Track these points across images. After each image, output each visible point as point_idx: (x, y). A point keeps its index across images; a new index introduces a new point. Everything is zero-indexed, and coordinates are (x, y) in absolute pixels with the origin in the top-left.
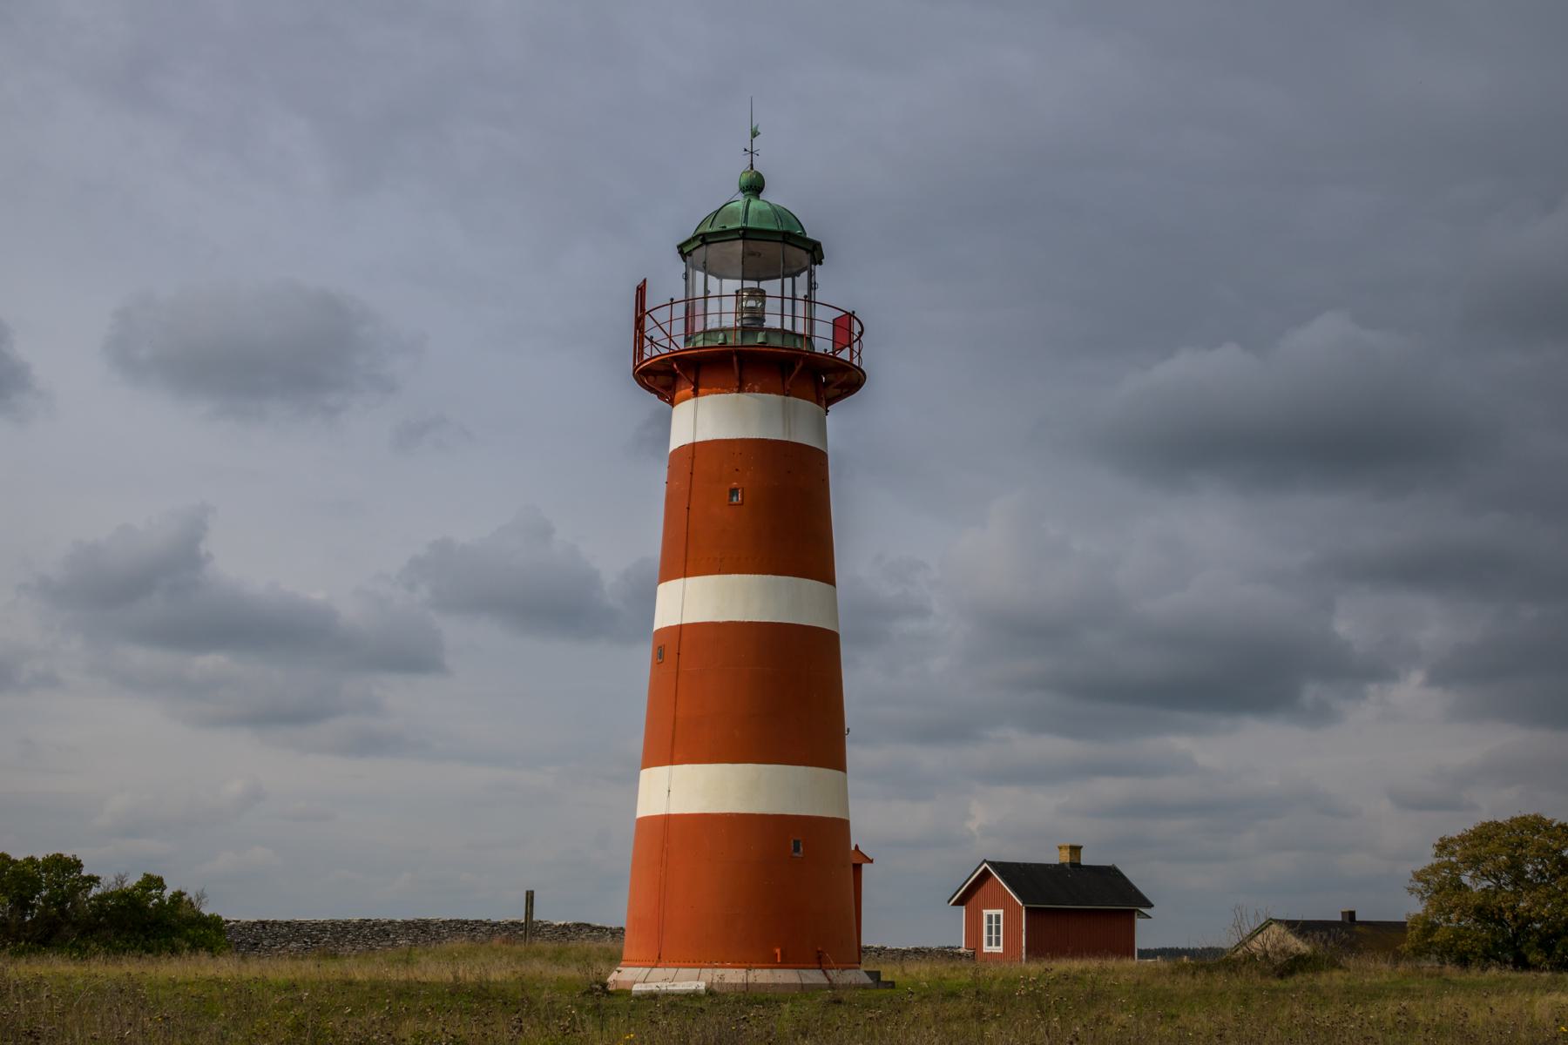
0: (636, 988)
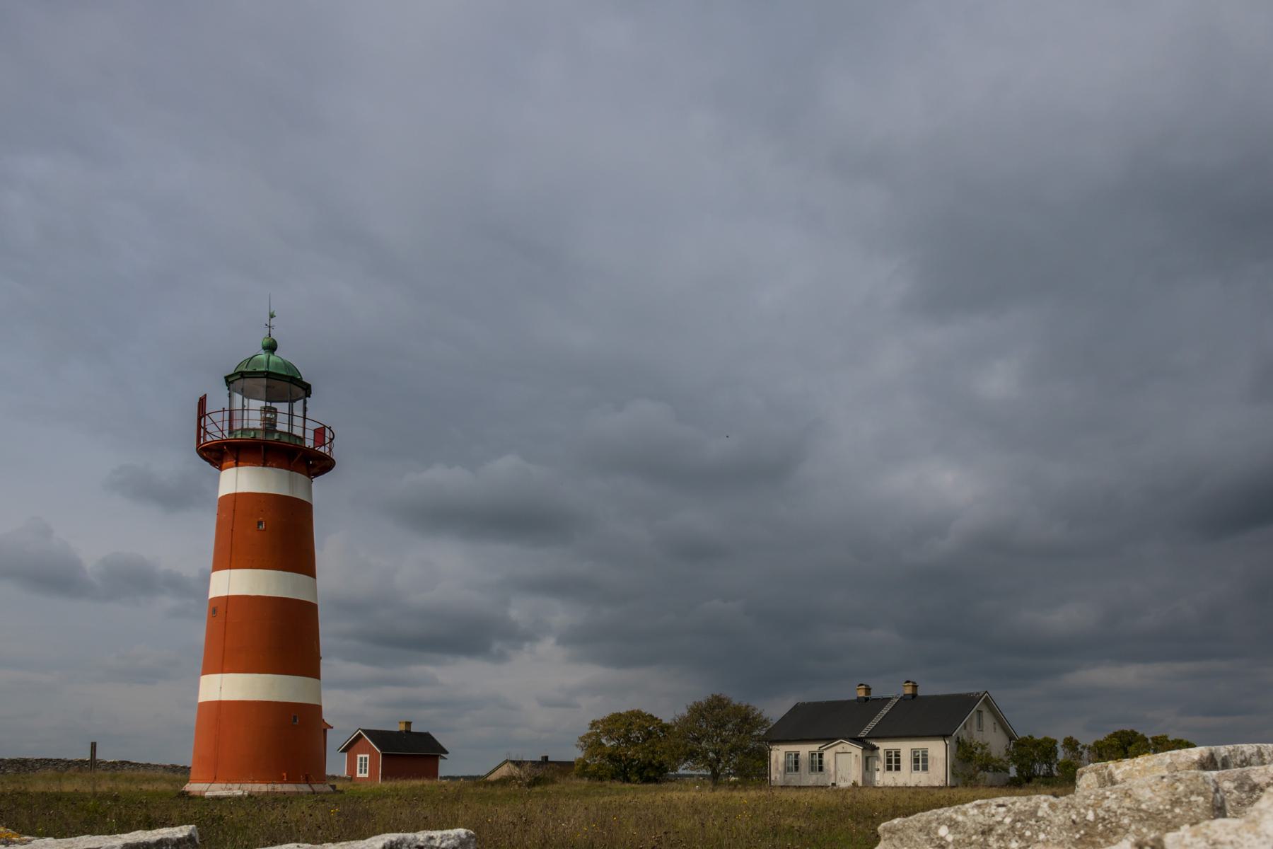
0: (207, 794)
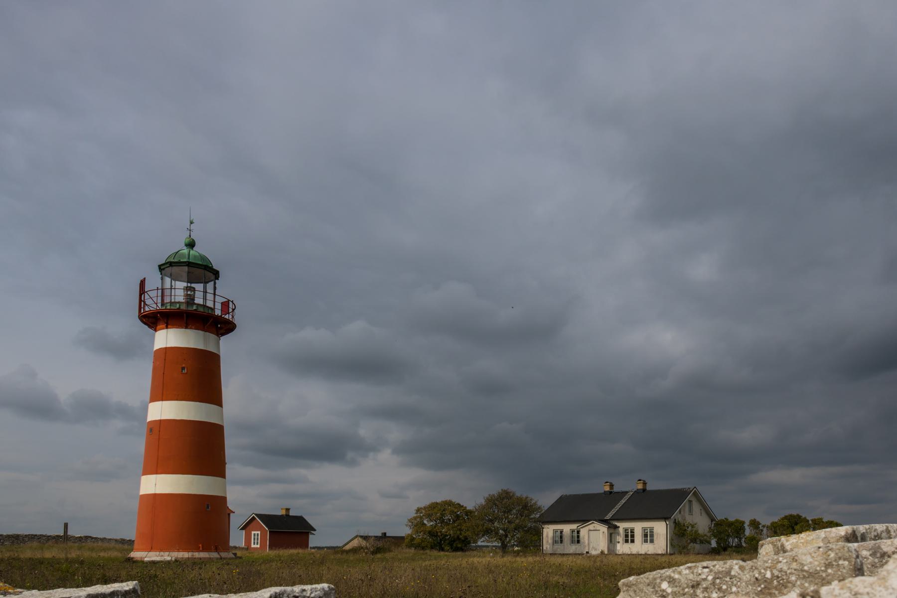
0: (146, 559)
